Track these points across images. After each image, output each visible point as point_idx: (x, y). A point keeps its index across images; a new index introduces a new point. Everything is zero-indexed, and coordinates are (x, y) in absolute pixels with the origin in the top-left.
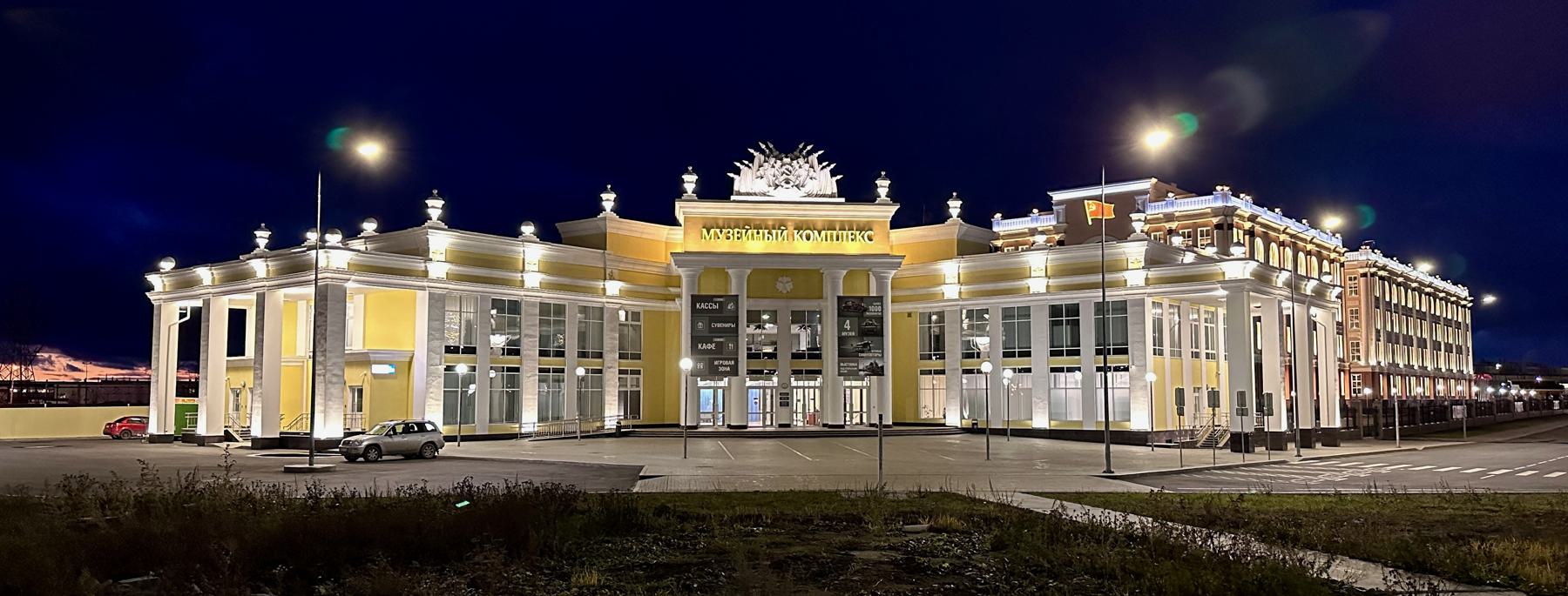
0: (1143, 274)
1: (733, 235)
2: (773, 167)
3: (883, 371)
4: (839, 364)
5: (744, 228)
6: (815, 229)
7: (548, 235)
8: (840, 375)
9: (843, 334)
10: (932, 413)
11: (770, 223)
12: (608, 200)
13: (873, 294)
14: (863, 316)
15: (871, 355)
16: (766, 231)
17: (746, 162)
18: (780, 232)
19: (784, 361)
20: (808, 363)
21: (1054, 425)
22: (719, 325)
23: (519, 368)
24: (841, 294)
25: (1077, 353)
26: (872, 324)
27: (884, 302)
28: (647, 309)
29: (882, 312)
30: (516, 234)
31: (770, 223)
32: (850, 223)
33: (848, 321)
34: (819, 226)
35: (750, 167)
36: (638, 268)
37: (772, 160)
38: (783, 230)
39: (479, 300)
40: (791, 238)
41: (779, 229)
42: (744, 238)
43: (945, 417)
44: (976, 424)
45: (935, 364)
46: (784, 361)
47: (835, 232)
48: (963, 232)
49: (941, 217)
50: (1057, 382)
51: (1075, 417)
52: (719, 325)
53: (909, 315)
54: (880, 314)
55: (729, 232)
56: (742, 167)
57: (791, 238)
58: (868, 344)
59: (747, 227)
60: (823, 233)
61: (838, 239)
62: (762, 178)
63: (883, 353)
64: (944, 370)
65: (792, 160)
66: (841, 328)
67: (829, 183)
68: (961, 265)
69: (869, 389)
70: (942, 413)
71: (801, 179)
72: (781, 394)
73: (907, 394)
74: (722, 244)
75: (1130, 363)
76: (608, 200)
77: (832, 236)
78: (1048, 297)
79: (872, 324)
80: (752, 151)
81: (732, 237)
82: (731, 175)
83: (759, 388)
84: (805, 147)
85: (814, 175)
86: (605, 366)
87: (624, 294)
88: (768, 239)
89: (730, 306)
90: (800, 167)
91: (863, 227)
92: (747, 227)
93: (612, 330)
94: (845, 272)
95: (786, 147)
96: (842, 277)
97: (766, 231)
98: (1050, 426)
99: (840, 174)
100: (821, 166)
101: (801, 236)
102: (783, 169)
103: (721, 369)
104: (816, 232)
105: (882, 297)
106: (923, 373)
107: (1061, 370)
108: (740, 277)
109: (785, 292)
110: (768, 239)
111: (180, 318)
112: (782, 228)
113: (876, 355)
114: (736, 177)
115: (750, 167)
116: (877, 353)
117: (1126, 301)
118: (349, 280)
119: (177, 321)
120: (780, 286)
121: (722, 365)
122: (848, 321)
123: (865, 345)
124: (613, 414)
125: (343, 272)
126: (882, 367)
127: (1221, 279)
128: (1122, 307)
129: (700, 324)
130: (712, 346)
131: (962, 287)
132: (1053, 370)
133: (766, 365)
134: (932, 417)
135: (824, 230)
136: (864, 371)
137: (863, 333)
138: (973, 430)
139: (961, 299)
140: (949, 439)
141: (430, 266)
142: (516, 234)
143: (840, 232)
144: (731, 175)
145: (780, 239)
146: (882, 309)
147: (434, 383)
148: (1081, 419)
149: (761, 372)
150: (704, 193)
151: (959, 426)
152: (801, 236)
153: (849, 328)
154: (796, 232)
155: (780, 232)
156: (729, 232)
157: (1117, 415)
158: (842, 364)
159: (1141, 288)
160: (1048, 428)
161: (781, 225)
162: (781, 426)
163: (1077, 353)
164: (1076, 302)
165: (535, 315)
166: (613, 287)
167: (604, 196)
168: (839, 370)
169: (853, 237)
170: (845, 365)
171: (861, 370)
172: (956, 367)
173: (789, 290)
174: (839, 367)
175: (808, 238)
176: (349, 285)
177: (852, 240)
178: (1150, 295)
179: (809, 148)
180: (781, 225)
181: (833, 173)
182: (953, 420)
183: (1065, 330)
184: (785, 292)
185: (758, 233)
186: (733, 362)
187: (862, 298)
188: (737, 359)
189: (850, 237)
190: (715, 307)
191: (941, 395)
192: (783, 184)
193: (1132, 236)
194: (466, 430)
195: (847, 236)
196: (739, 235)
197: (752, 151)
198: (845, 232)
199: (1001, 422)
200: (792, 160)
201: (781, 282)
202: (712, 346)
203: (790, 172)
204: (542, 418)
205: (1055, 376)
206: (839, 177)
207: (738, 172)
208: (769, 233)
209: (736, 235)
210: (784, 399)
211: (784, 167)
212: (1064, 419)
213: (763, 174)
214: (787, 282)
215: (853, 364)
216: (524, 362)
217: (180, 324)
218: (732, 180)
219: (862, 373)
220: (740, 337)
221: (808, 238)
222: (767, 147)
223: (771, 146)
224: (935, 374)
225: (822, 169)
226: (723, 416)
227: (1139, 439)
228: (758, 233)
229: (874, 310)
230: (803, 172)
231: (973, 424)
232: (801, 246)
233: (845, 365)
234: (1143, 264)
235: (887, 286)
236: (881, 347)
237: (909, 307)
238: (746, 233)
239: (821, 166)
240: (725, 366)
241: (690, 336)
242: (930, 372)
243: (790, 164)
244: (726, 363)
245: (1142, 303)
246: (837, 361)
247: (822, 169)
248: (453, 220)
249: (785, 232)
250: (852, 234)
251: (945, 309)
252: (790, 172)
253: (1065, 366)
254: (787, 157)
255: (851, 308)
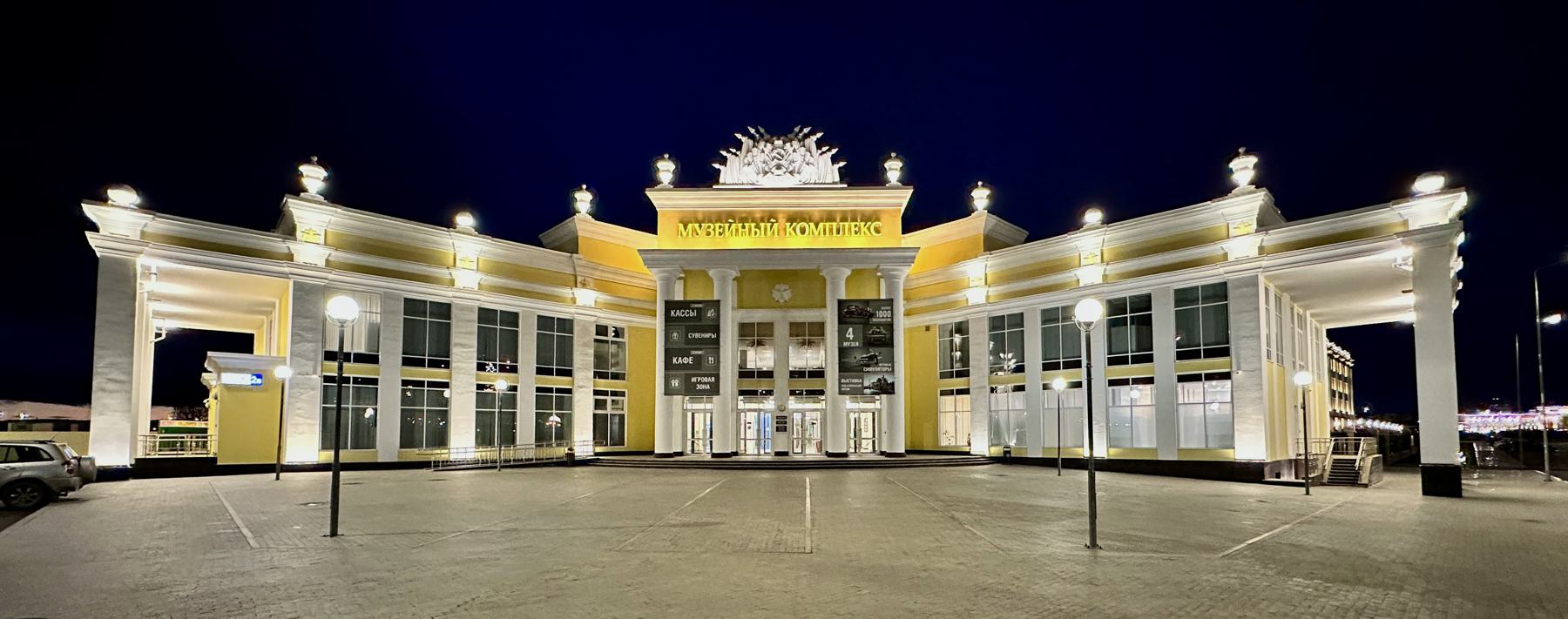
0: (1257, 240)
1: (714, 230)
2: (763, 151)
3: (893, 389)
4: (840, 381)
5: (727, 222)
6: (811, 221)
7: (491, 227)
8: (841, 393)
9: (845, 344)
10: (953, 439)
11: (758, 216)
12: (583, 200)
13: (883, 296)
14: (868, 323)
15: (879, 369)
16: (753, 225)
17: (734, 151)
18: (769, 225)
19: (781, 383)
20: (808, 383)
21: (1114, 454)
22: (697, 335)
23: (448, 383)
24: (843, 297)
25: (1149, 359)
26: (879, 333)
27: (894, 306)
28: (634, 325)
29: (892, 318)
30: (449, 224)
31: (758, 216)
32: (854, 212)
33: (851, 329)
34: (816, 216)
35: (737, 155)
36: (618, 278)
37: (762, 144)
38: (773, 223)
39: (387, 297)
40: (782, 232)
41: (769, 221)
42: (727, 233)
43: (969, 445)
44: (1009, 452)
45: (958, 383)
46: (781, 383)
47: (834, 224)
48: (989, 227)
49: (965, 210)
50: (1117, 399)
51: (1145, 443)
52: (697, 335)
53: (928, 328)
54: (890, 320)
55: (709, 227)
56: (728, 155)
57: (782, 232)
58: (875, 356)
59: (730, 220)
60: (821, 225)
61: (838, 232)
62: (749, 164)
63: (893, 367)
64: (969, 389)
65: (784, 143)
66: (842, 336)
67: (829, 171)
68: (989, 263)
69: (880, 411)
70: (966, 440)
71: (797, 165)
72: (777, 418)
73: (924, 416)
74: (702, 241)
75: (1234, 368)
76: (583, 200)
77: (831, 230)
78: (1105, 289)
79: (879, 333)
80: (739, 136)
81: (712, 232)
82: (717, 166)
83: (755, 410)
84: (801, 130)
85: (812, 160)
86: (576, 385)
87: (598, 306)
88: (756, 233)
89: (710, 313)
90: (794, 151)
91: (869, 218)
92: (730, 220)
93: (585, 345)
94: (848, 272)
95: (779, 127)
96: (845, 277)
97: (753, 225)
98: (1108, 455)
99: (834, 148)
100: (820, 152)
101: (794, 230)
102: (774, 154)
103: (699, 387)
104: (812, 224)
105: (892, 300)
106: (943, 393)
107: (1125, 382)
108: (723, 279)
109: (782, 301)
110: (756, 233)
111: (156, 338)
112: (772, 220)
113: (885, 369)
114: (722, 168)
115: (737, 155)
116: (884, 367)
117: (1226, 283)
118: (141, 253)
119: (153, 339)
120: (776, 295)
121: (700, 383)
122: (851, 329)
123: (871, 358)
124: (583, 442)
125: (127, 241)
126: (893, 384)
127: (1401, 229)
128: (1219, 291)
129: (675, 334)
130: (688, 360)
131: (990, 289)
132: (1112, 383)
133: (763, 385)
134: (954, 444)
135: (822, 221)
136: (870, 388)
137: (869, 343)
138: (1007, 460)
139: (988, 303)
140: (976, 472)
141: (293, 246)
142: (449, 224)
143: (841, 224)
144: (717, 166)
145: (769, 233)
146: (892, 314)
147: (303, 397)
148: (1154, 446)
149: (754, 393)
150: (685, 180)
151: (987, 455)
152: (794, 230)
153: (851, 337)
154: (789, 224)
155: (769, 225)
156: (709, 227)
157: (1210, 439)
158: (843, 381)
159: (1253, 259)
160: (1106, 458)
161: (770, 217)
162: (777, 454)
163: (1149, 359)
164: (1145, 291)
165: (475, 321)
166: (586, 297)
167: (578, 195)
168: (840, 388)
169: (857, 229)
170: (847, 381)
171: (866, 388)
172: (982, 385)
173: (787, 299)
174: (840, 383)
175: (803, 231)
176: (141, 262)
177: (856, 233)
178: (1266, 269)
179: (806, 130)
180: (770, 217)
181: (834, 160)
182: (981, 446)
183: (1130, 331)
184: (782, 301)
185: (744, 227)
186: (713, 379)
187: (867, 302)
188: (719, 374)
189: (853, 229)
190: (692, 314)
191: (964, 419)
192: (774, 170)
193: (1233, 191)
194: (510, 453)
195: (850, 229)
196: (721, 230)
197: (739, 136)
198: (847, 224)
199: (1041, 449)
200: (784, 143)
201: (779, 290)
202: (688, 360)
203: (783, 156)
204: (484, 439)
205: (1113, 390)
206: (842, 164)
207: (724, 161)
208: (756, 227)
209: (717, 230)
210: (782, 423)
211: (775, 151)
212: (1129, 445)
213: (751, 160)
214: (785, 290)
215: (856, 381)
216: (454, 376)
217: (156, 343)
218: (719, 171)
219: (867, 391)
220: (721, 349)
221: (803, 231)
222: (757, 131)
223: (762, 130)
224: (957, 394)
225: (821, 154)
226: (711, 442)
227: (1251, 473)
228: (744, 227)
229: (882, 315)
230: (797, 157)
231: (1005, 452)
232: (796, 241)
233: (847, 381)
234: (1255, 226)
235: (898, 287)
236: (891, 360)
237: (925, 319)
238: (729, 227)
239: (820, 152)
240: (705, 383)
241: (663, 349)
242: (951, 393)
243: (782, 148)
244: (705, 379)
245: (1253, 282)
246: (837, 377)
247: (821, 154)
248: (337, 194)
249: (776, 225)
250: (856, 226)
251: (969, 317)
252: (783, 156)
253: (1131, 377)
254: (779, 139)
255: (852, 313)
